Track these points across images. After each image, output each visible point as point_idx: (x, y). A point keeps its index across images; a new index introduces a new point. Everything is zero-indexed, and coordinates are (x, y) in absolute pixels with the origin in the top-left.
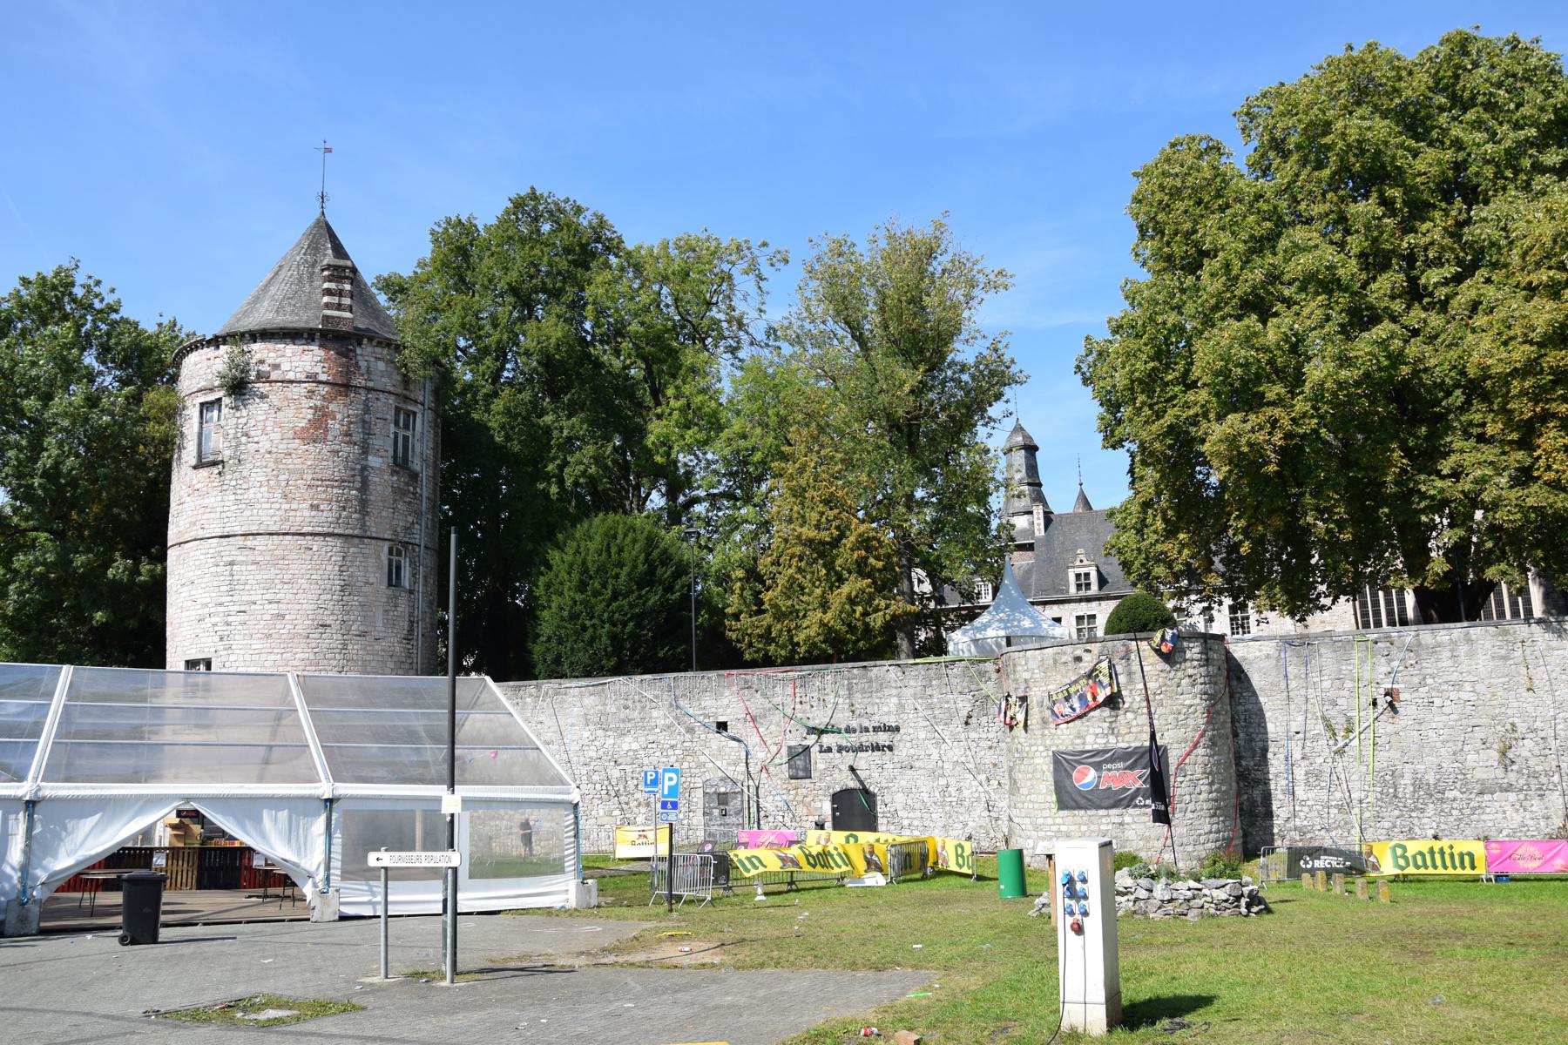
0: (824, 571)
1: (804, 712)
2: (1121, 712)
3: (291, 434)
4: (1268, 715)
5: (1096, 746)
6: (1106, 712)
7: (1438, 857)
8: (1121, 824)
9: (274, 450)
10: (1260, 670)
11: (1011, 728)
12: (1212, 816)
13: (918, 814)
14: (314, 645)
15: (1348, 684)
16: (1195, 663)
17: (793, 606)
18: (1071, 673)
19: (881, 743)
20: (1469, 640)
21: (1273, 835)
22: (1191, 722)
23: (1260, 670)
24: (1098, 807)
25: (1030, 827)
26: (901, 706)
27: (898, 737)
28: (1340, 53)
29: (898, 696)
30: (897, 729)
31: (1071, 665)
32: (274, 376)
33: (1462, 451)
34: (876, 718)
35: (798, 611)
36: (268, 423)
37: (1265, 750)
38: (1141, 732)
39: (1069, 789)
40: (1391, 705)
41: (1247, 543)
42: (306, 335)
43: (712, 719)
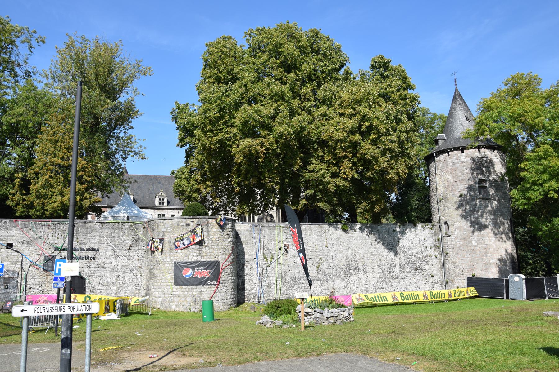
0: (63, 179)
1: (54, 240)
2: (204, 247)
4: (245, 251)
5: (193, 260)
6: (198, 247)
7: (377, 298)
8: (201, 292)
10: (244, 235)
11: (153, 252)
12: (232, 289)
13: (105, 287)
15: (273, 242)
16: (230, 230)
17: (46, 193)
18: (184, 230)
19: (90, 256)
20: (311, 229)
21: (245, 296)
22: (227, 252)
23: (244, 235)
24: (192, 285)
25: (161, 293)
26: (100, 240)
27: (98, 254)
28: (285, 23)
29: (100, 236)
30: (98, 250)
31: (185, 227)
33: (316, 164)
34: (88, 245)
35: (48, 195)
37: (244, 265)
38: (211, 255)
39: (181, 277)
40: (286, 250)
41: (238, 188)
43: (4, 242)
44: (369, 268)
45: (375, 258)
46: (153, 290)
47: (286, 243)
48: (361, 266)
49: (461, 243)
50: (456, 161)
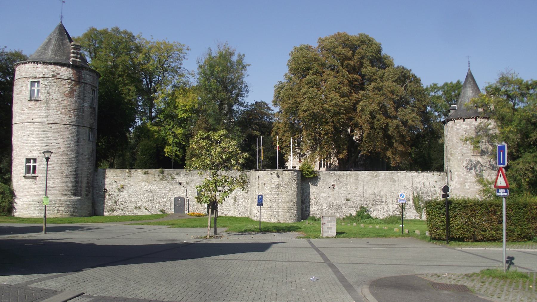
3: (63, 95)
9: (58, 99)
13: (228, 207)
14: (69, 156)
20: (350, 175)
32: (58, 76)
36: (56, 91)
40: (334, 188)
42: (67, 65)
43: (178, 182)
44: (390, 201)
45: (395, 194)
46: (253, 210)
47: (333, 184)
48: (384, 199)
49: (459, 186)
50: (459, 127)
